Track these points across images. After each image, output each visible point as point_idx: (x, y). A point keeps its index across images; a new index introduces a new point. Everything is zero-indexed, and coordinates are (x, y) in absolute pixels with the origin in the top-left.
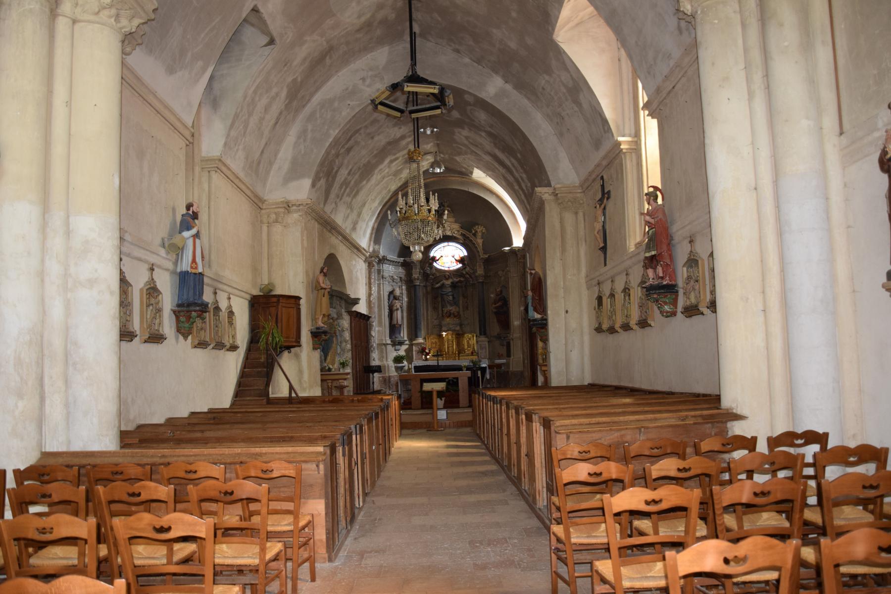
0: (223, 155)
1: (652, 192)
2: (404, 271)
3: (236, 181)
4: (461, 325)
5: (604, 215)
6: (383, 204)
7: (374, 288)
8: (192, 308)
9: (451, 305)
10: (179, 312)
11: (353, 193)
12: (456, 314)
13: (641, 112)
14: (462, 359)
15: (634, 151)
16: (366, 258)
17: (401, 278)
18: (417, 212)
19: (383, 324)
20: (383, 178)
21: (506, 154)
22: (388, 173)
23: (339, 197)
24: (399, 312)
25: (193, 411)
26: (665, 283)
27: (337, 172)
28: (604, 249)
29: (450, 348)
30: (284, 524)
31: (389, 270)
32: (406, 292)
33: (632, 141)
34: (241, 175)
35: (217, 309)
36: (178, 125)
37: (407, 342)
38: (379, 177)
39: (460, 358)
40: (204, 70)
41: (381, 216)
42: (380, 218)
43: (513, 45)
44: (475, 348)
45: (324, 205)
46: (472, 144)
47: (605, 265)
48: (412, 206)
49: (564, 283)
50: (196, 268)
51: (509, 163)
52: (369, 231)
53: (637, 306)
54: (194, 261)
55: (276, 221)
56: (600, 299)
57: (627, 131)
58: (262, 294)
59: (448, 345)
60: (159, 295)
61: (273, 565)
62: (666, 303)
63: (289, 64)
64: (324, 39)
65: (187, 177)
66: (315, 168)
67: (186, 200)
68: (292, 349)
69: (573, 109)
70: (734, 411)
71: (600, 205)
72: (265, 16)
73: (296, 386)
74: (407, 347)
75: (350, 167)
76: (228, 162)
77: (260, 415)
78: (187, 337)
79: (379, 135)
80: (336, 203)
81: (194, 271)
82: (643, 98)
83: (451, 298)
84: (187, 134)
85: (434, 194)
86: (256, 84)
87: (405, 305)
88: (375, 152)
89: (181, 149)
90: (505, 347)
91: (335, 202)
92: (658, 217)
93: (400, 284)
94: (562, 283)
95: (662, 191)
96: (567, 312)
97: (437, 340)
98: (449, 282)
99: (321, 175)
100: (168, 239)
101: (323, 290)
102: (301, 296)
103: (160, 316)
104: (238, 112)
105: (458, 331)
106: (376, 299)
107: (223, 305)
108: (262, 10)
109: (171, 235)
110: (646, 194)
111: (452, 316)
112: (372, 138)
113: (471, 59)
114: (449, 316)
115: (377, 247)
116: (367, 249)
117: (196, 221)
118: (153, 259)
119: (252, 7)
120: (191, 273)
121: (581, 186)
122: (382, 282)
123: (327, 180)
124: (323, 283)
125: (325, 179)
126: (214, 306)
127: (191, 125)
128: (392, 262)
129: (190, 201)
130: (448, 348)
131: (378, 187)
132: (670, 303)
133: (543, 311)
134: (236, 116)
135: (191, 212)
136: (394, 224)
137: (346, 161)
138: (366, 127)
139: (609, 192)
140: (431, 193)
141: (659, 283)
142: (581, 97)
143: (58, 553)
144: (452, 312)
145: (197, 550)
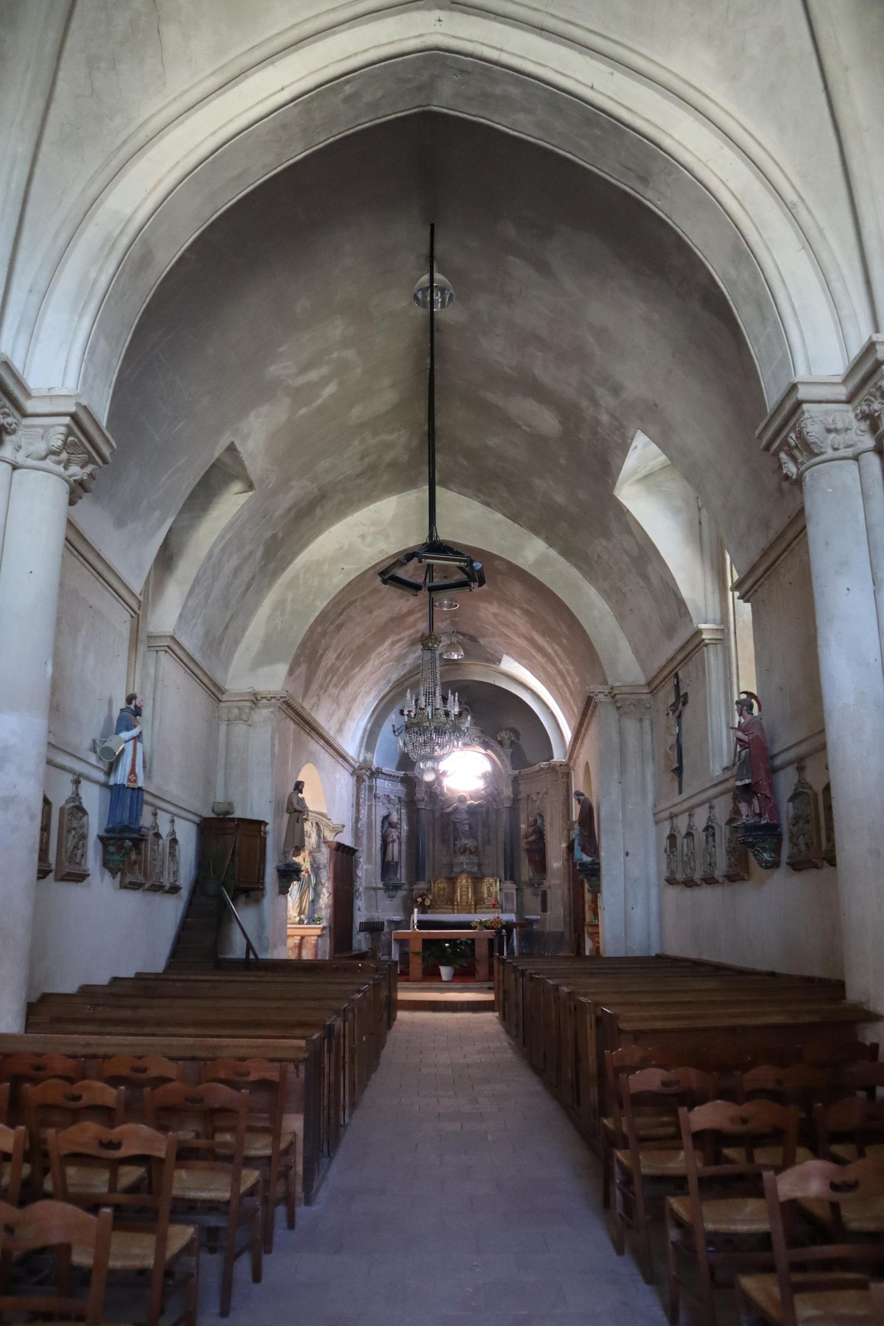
0: (176, 631)
1: (744, 700)
2: (404, 789)
3: (191, 665)
4: (479, 865)
5: (679, 725)
6: (380, 698)
7: (363, 811)
8: (127, 835)
9: (466, 837)
10: (108, 839)
11: (342, 683)
12: (473, 850)
13: (730, 594)
15: (720, 642)
16: (355, 770)
17: (399, 798)
18: (430, 717)
19: (374, 860)
20: (382, 665)
21: (548, 638)
22: (388, 657)
23: (324, 688)
24: (396, 845)
25: (115, 975)
26: (763, 822)
27: (321, 656)
28: (679, 771)
29: (464, 897)
30: (260, 1147)
31: (383, 786)
32: (405, 817)
33: (717, 630)
34: (198, 657)
35: (158, 835)
36: (123, 592)
37: (406, 886)
38: (376, 663)
39: (478, 910)
40: (161, 521)
41: (376, 713)
42: (374, 717)
43: (560, 499)
44: (498, 897)
45: (303, 699)
46: (502, 623)
47: (680, 792)
48: (423, 709)
49: (623, 815)
50: (135, 781)
51: (550, 651)
52: (360, 733)
53: (724, 853)
54: (133, 771)
55: (239, 718)
56: (672, 838)
57: (710, 616)
58: (214, 816)
59: (461, 892)
60: (83, 816)
61: (248, 1201)
62: (764, 850)
63: (267, 517)
64: (315, 485)
65: (129, 659)
66: (294, 650)
67: (127, 691)
68: (251, 893)
69: (638, 584)
70: (865, 1007)
71: (674, 712)
72: (244, 456)
73: (255, 945)
75: (339, 650)
76: (183, 640)
77: (207, 985)
78: (117, 874)
79: (379, 608)
80: (318, 695)
81: (132, 785)
82: (732, 576)
83: (467, 828)
84: (134, 604)
85: (453, 693)
86: (224, 542)
87: (404, 834)
88: (374, 630)
89: (125, 622)
90: (539, 898)
91: (318, 695)
92: (753, 733)
93: (398, 806)
94: (620, 815)
95: (759, 698)
96: (627, 854)
97: (445, 885)
99: (302, 659)
100: (101, 741)
101: (297, 814)
102: (267, 821)
103: (83, 845)
104: (200, 575)
105: (475, 873)
106: (365, 825)
107: (164, 830)
108: (240, 448)
109: (105, 735)
110: (737, 703)
111: (467, 852)
112: (371, 612)
113: (504, 514)
114: (463, 853)
115: (369, 755)
116: (356, 758)
117: (138, 717)
118: (80, 767)
119: (227, 443)
120: (128, 788)
121: (649, 684)
122: (374, 803)
123: (309, 668)
124: (297, 804)
125: (306, 665)
126: (171, 838)
127: (139, 593)
128: (389, 776)
129: (131, 692)
130: (461, 896)
131: (374, 676)
132: (772, 850)
133: (595, 852)
134: (197, 581)
135: (132, 706)
136: (400, 731)
137: (334, 642)
138: (364, 598)
139: (686, 695)
140: (450, 692)
141: (755, 822)
142: (650, 569)
145: (146, 1176)
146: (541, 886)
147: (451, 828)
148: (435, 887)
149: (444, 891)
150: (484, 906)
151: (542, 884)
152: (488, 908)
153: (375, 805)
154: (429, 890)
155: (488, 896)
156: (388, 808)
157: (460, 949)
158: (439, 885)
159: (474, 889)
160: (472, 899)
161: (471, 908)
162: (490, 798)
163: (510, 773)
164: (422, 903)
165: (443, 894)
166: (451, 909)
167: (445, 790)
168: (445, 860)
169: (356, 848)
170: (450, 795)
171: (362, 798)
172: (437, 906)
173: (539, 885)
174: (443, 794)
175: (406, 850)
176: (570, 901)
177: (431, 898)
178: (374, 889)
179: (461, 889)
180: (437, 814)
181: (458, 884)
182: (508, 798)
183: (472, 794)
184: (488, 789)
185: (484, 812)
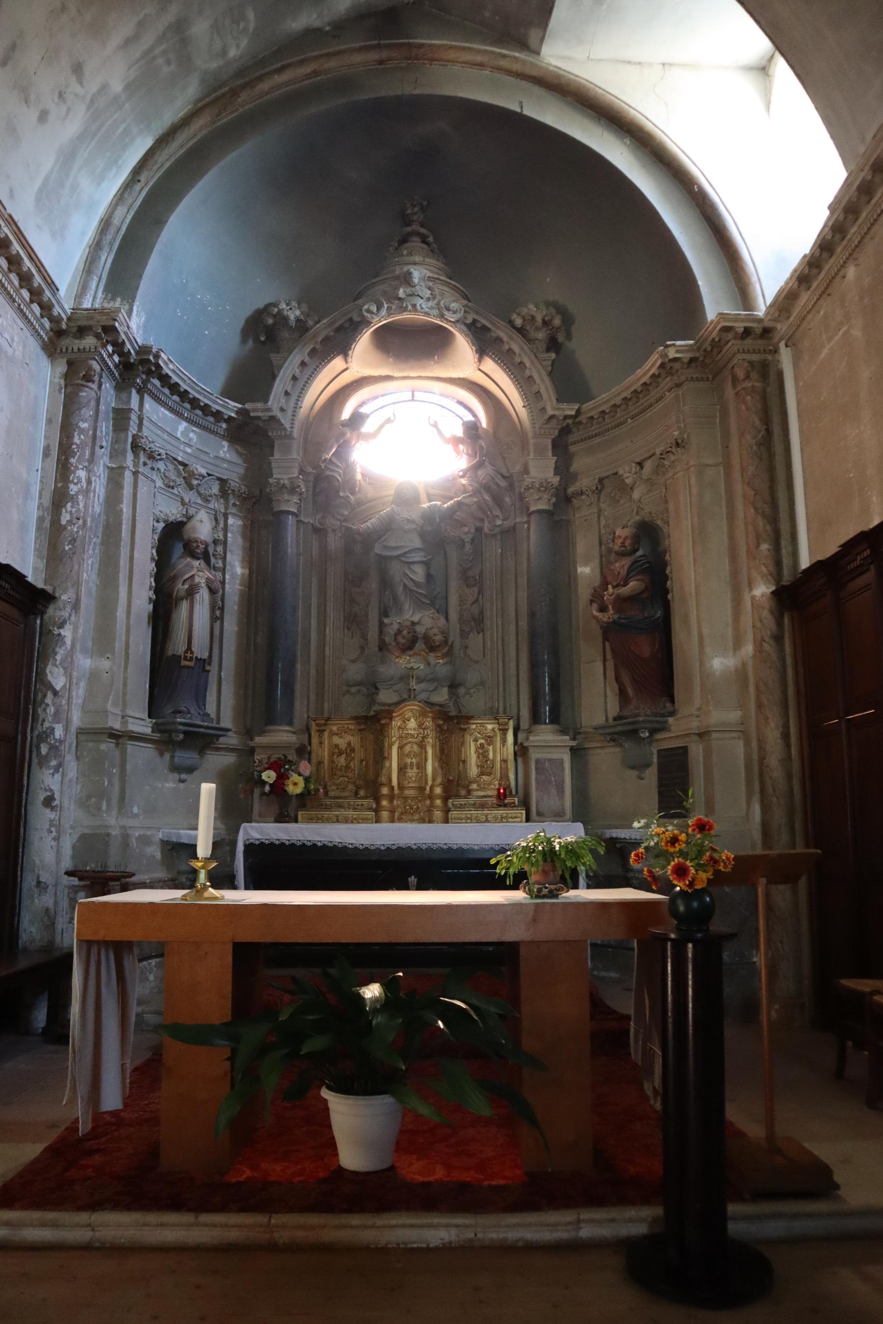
4: (453, 686)
7: (97, 509)
9: (419, 604)
12: (439, 638)
14: (459, 820)
16: (59, 333)
29: (412, 773)
32: (240, 540)
37: (232, 740)
39: (453, 814)
59: (401, 756)
74: (229, 759)
83: (419, 574)
87: (233, 588)
90: (651, 775)
97: (354, 740)
111: (420, 645)
114: (408, 647)
130: (402, 769)
143: (488, 777)
144: (420, 630)
146: (659, 736)
147: (373, 585)
148: (321, 743)
149: (349, 759)
150: (471, 801)
151: (664, 728)
152: (483, 806)
153: (135, 474)
154: (303, 751)
155: (482, 773)
156: (183, 503)
157: (450, 1014)
158: (336, 740)
159: (442, 751)
160: (434, 780)
161: (432, 805)
162: (487, 497)
163: (550, 412)
164: (278, 788)
165: (347, 767)
166: (370, 809)
167: (359, 477)
168: (356, 671)
169: (49, 589)
170: (371, 493)
171: (82, 431)
172: (328, 802)
173: (653, 732)
174: (350, 485)
175: (240, 634)
176: (789, 776)
177: (307, 773)
178: (116, 736)
179: (401, 748)
180: (334, 542)
181: (394, 733)
182: (544, 486)
183: (432, 492)
184: (481, 473)
185: (467, 538)
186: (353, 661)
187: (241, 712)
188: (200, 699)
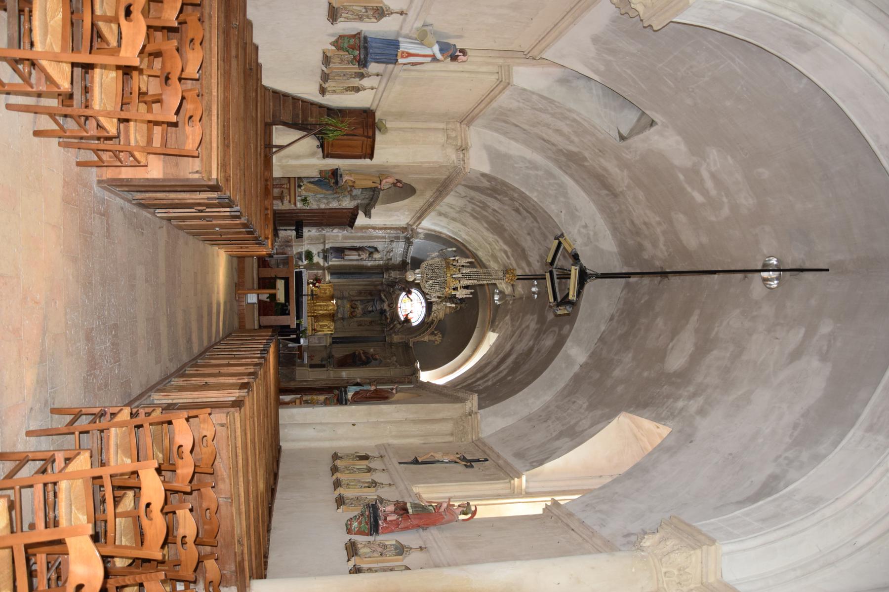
9: (363, 309)
29: (319, 308)
37: (326, 265)
74: (322, 264)
87: (364, 263)
98: (385, 306)
111: (352, 310)
130: (320, 306)
149: (323, 293)
152: (312, 325)
175: (353, 265)
186: (349, 293)
187: (332, 266)
188: (335, 257)
